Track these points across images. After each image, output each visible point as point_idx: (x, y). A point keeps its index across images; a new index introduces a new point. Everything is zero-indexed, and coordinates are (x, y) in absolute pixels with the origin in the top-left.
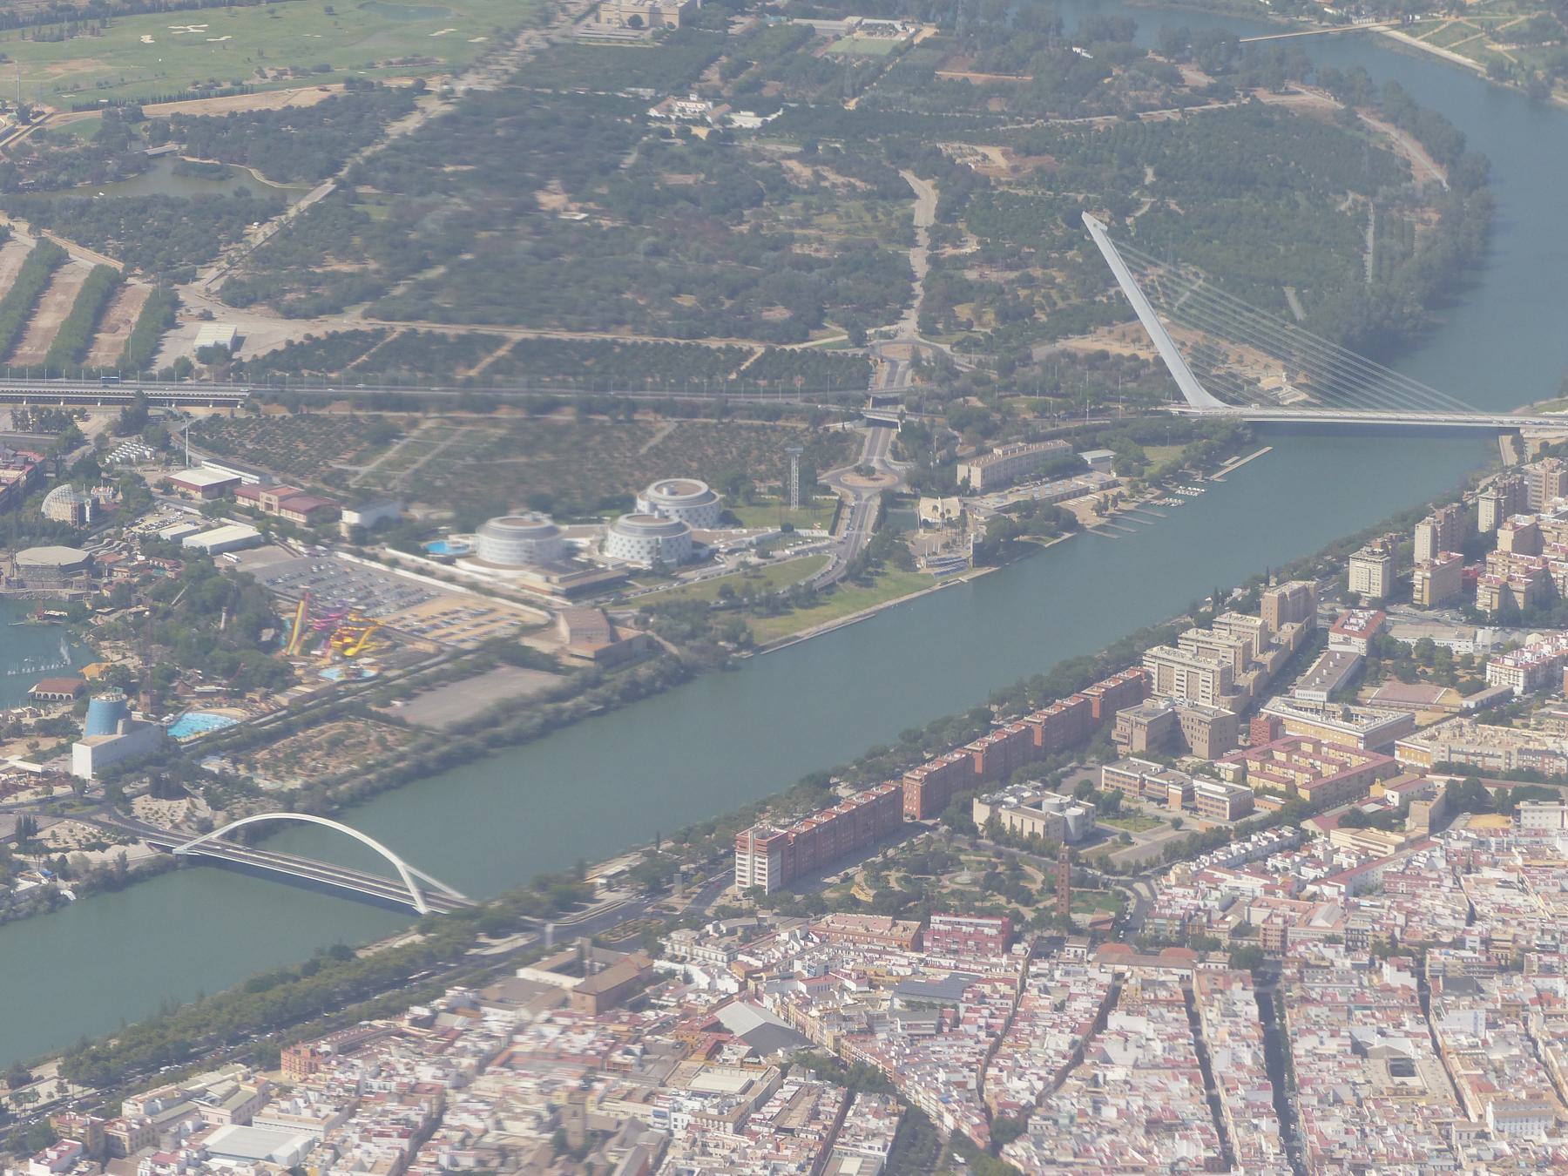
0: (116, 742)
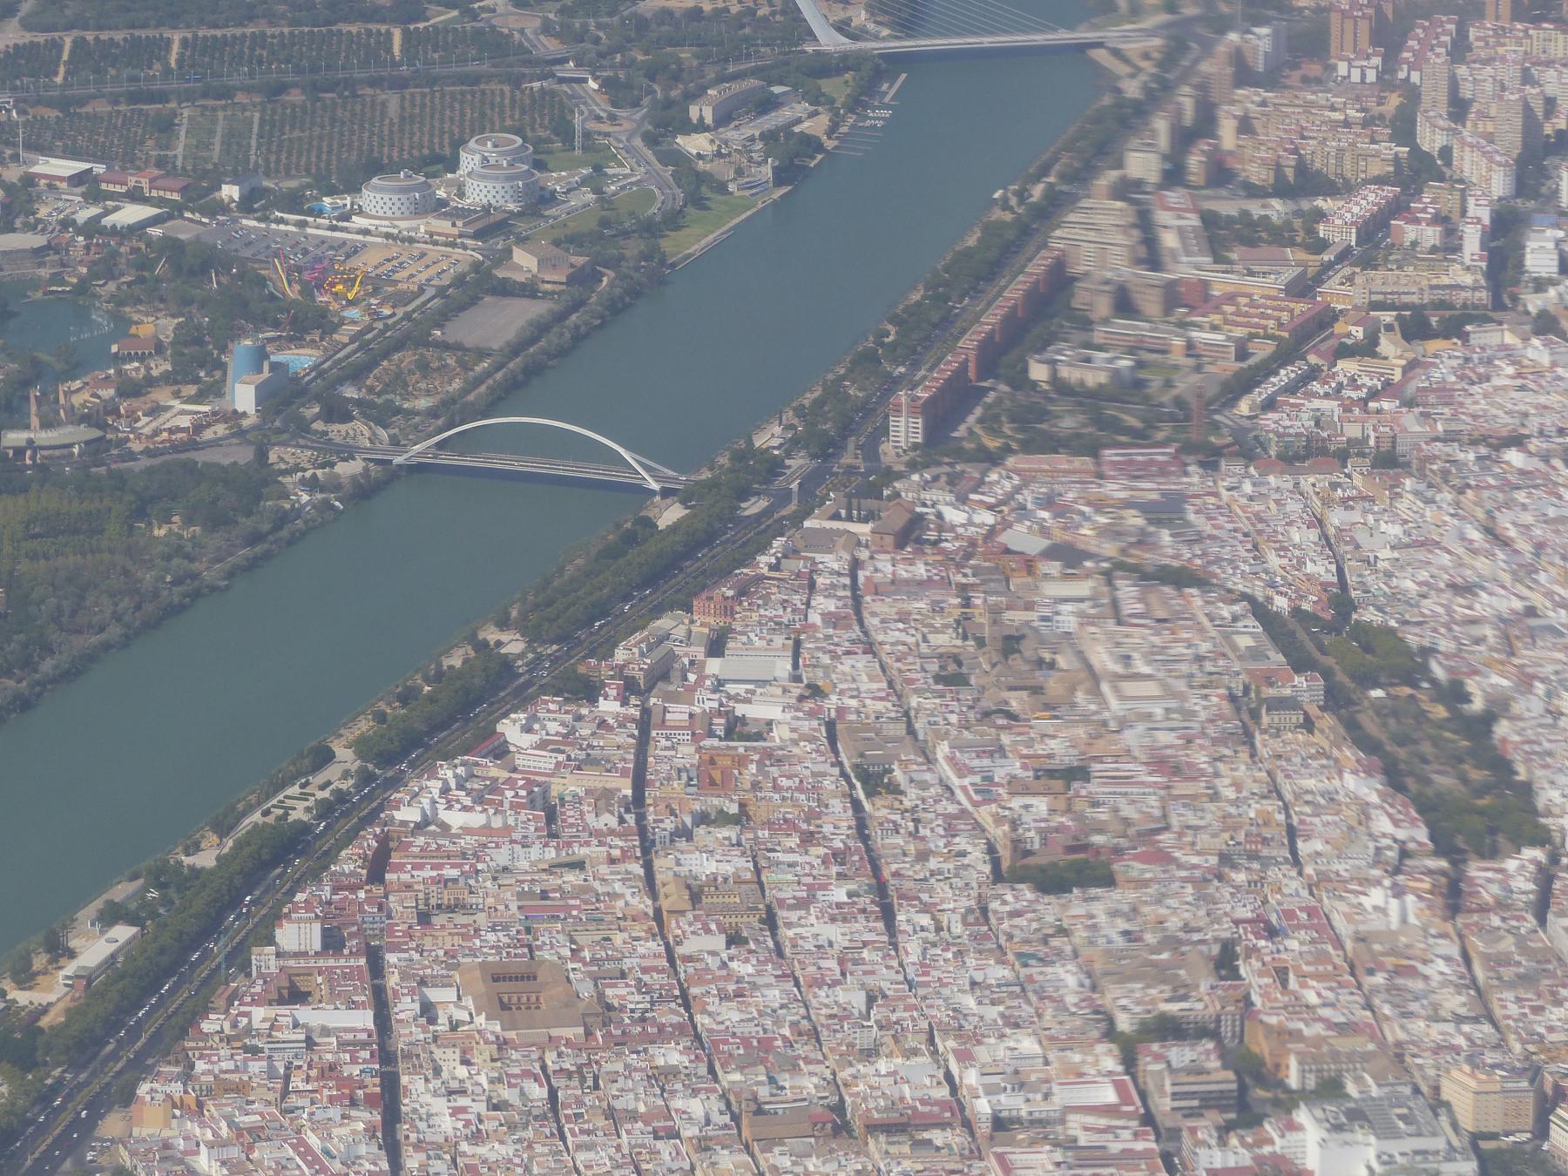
0: (268, 381)
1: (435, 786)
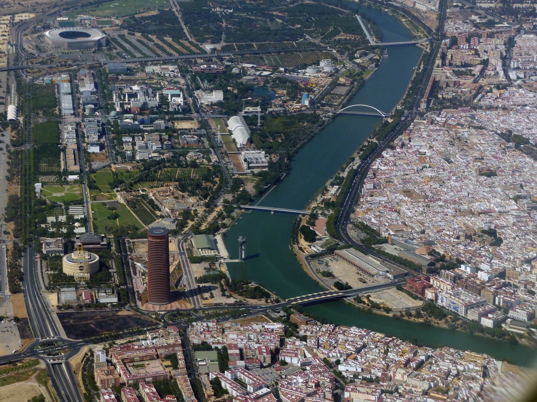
1: (378, 163)
